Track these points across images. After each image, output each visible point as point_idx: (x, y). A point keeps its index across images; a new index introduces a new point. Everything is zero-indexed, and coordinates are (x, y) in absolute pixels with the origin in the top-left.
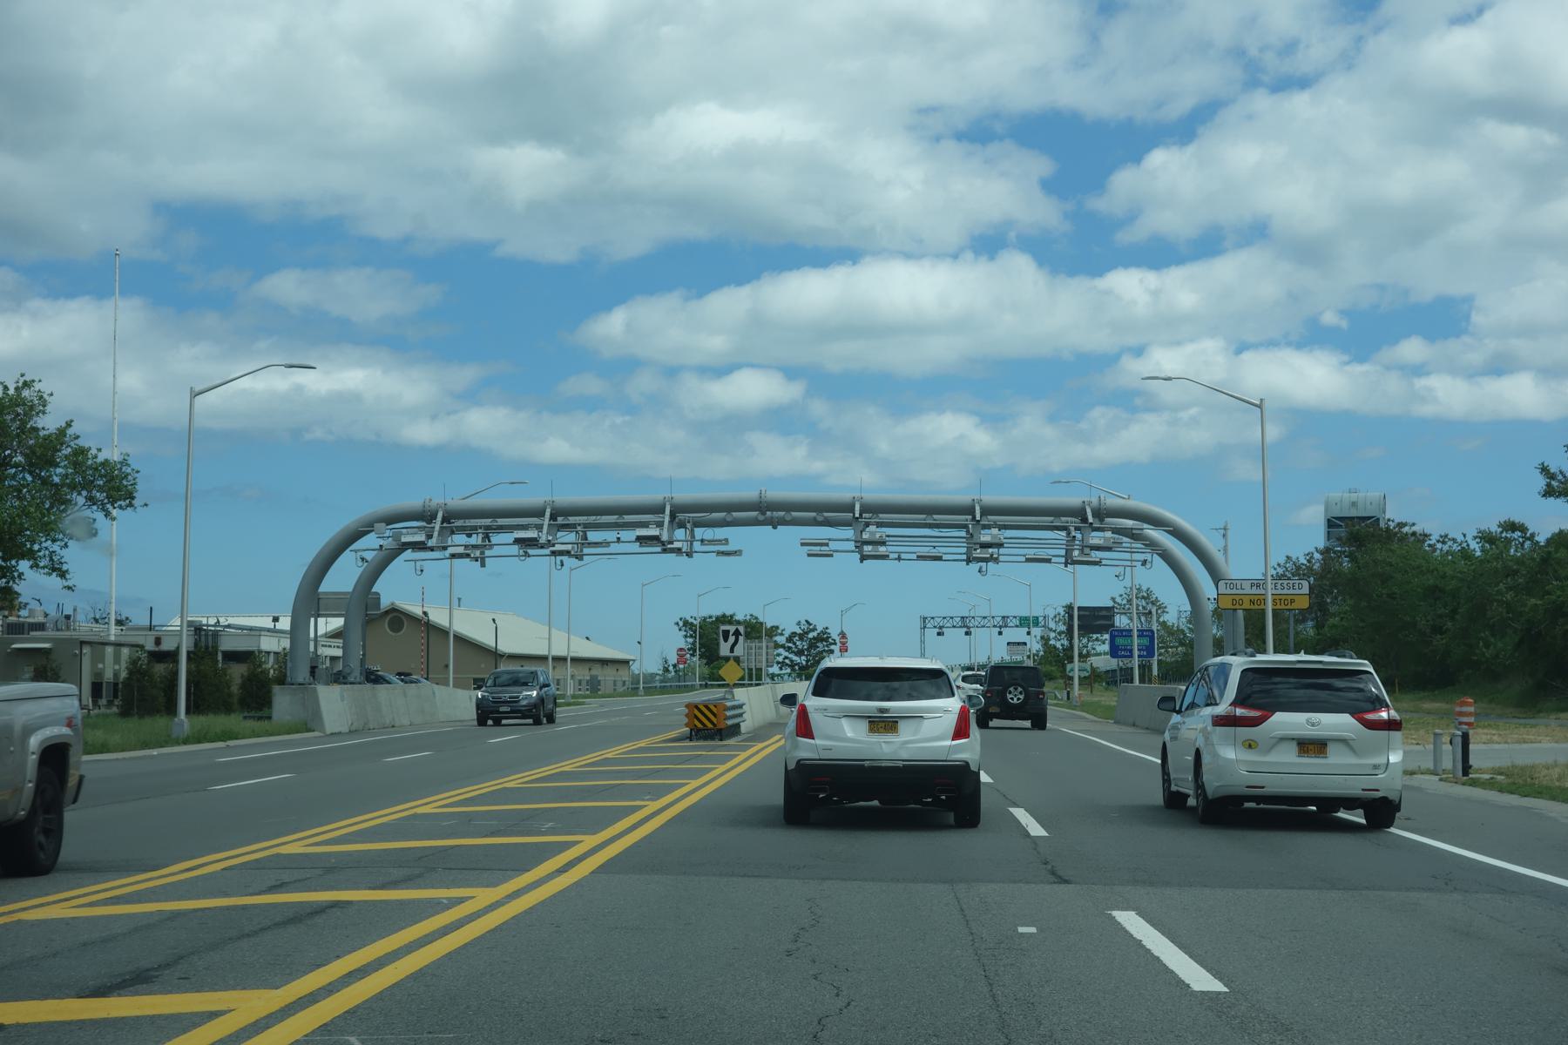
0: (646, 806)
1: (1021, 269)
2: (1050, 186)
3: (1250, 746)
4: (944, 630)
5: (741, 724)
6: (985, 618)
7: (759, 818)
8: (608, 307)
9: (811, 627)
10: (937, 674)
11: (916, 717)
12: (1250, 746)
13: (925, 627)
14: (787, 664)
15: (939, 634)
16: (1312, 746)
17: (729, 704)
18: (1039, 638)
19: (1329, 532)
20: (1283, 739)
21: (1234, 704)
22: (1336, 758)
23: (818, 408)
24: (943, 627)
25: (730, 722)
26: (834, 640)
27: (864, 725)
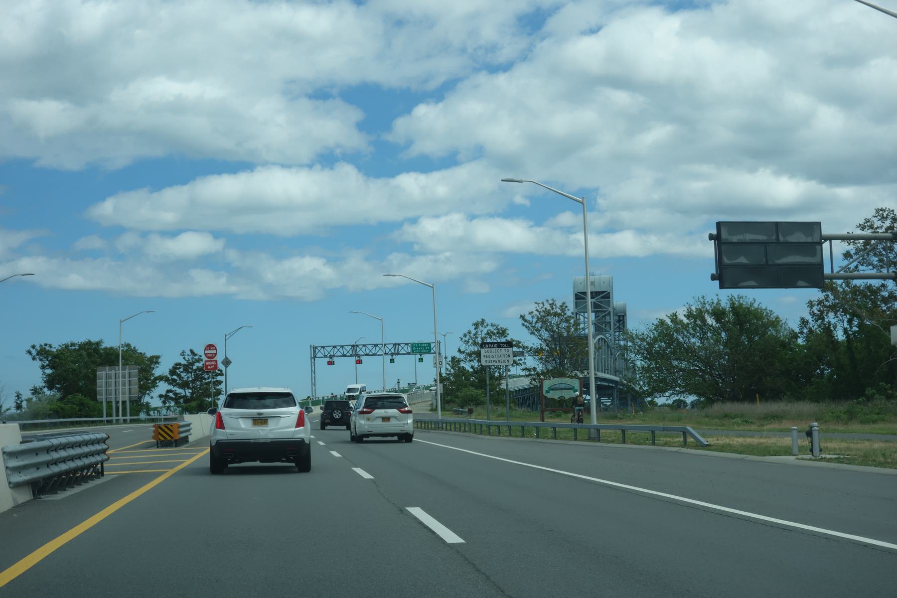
0: (167, 471)
1: (349, 173)
2: (361, 126)
3: (368, 420)
4: (335, 359)
5: (189, 436)
6: (376, 345)
8: (103, 199)
9: (196, 357)
12: (368, 419)
13: (315, 357)
14: (171, 398)
15: (330, 363)
16: (386, 419)
17: (181, 424)
18: (449, 359)
19: (576, 302)
20: (378, 417)
21: (363, 408)
22: (393, 422)
23: (232, 255)
24: (334, 356)
25: (182, 435)
26: (221, 371)
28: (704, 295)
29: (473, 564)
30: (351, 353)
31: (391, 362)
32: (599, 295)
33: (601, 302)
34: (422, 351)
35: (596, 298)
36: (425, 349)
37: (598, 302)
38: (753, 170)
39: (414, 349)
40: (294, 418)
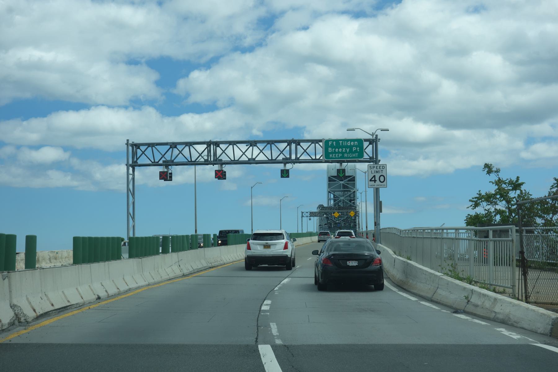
1: (151, 112)
2: (158, 83)
4: (174, 169)
7: (240, 269)
10: (281, 234)
11: (275, 244)
19: (329, 184)
23: (75, 162)
27: (262, 247)
30: (206, 158)
31: (282, 177)
32: (346, 179)
33: (348, 184)
34: (346, 155)
35: (344, 181)
36: (351, 151)
38: (400, 118)
39: (330, 150)
40: (283, 245)
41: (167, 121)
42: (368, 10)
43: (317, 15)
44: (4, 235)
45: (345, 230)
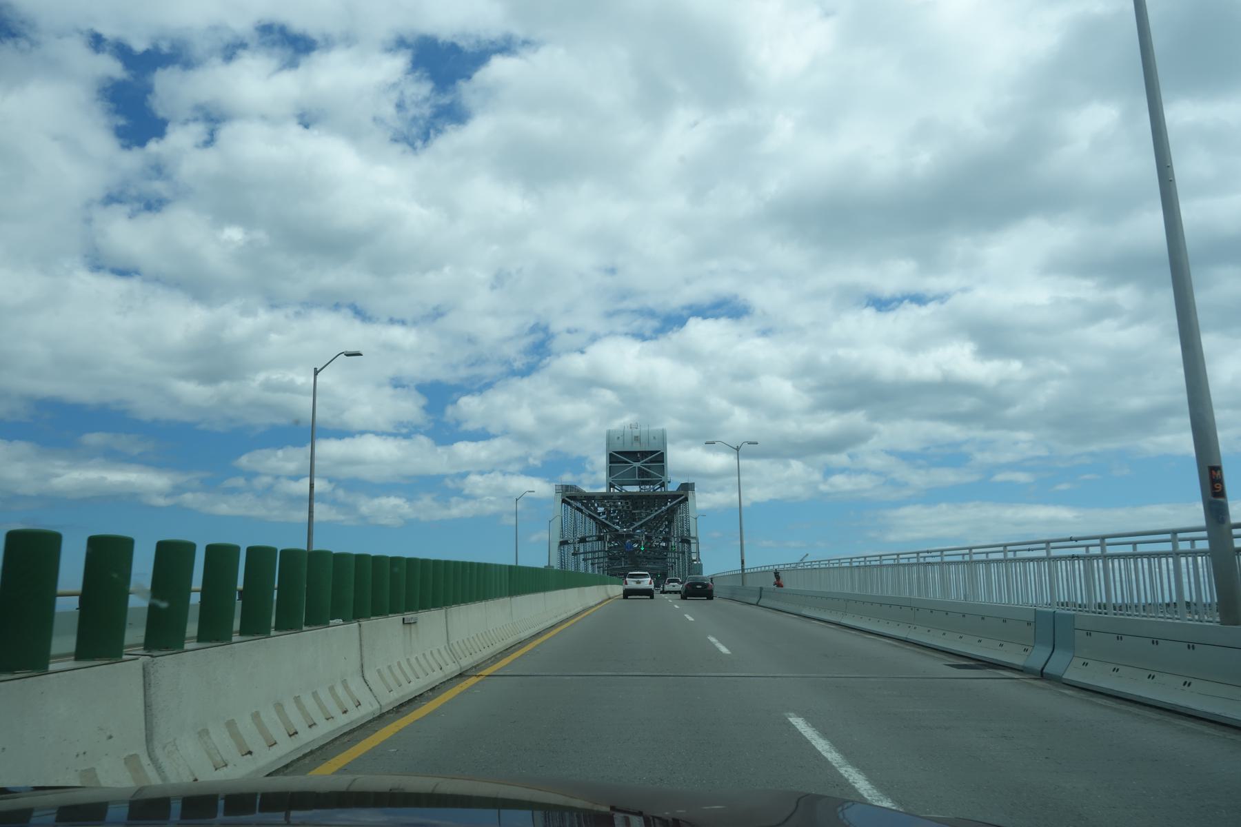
23: (341, 493)
28: (254, 755)
29: (672, 321)
32: (646, 457)
33: (649, 467)
37: (645, 466)
40: (649, 582)
41: (440, 450)
42: (648, 334)
43: (594, 338)
44: (387, 557)
45: (821, 745)
